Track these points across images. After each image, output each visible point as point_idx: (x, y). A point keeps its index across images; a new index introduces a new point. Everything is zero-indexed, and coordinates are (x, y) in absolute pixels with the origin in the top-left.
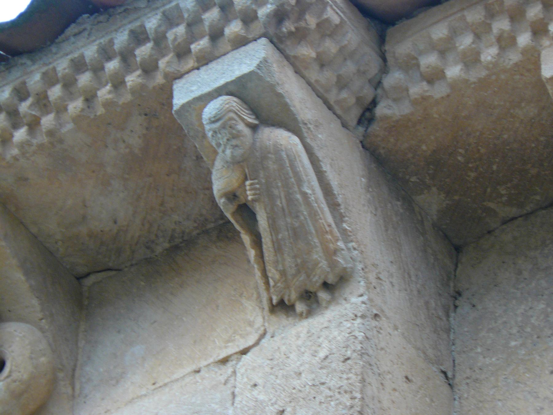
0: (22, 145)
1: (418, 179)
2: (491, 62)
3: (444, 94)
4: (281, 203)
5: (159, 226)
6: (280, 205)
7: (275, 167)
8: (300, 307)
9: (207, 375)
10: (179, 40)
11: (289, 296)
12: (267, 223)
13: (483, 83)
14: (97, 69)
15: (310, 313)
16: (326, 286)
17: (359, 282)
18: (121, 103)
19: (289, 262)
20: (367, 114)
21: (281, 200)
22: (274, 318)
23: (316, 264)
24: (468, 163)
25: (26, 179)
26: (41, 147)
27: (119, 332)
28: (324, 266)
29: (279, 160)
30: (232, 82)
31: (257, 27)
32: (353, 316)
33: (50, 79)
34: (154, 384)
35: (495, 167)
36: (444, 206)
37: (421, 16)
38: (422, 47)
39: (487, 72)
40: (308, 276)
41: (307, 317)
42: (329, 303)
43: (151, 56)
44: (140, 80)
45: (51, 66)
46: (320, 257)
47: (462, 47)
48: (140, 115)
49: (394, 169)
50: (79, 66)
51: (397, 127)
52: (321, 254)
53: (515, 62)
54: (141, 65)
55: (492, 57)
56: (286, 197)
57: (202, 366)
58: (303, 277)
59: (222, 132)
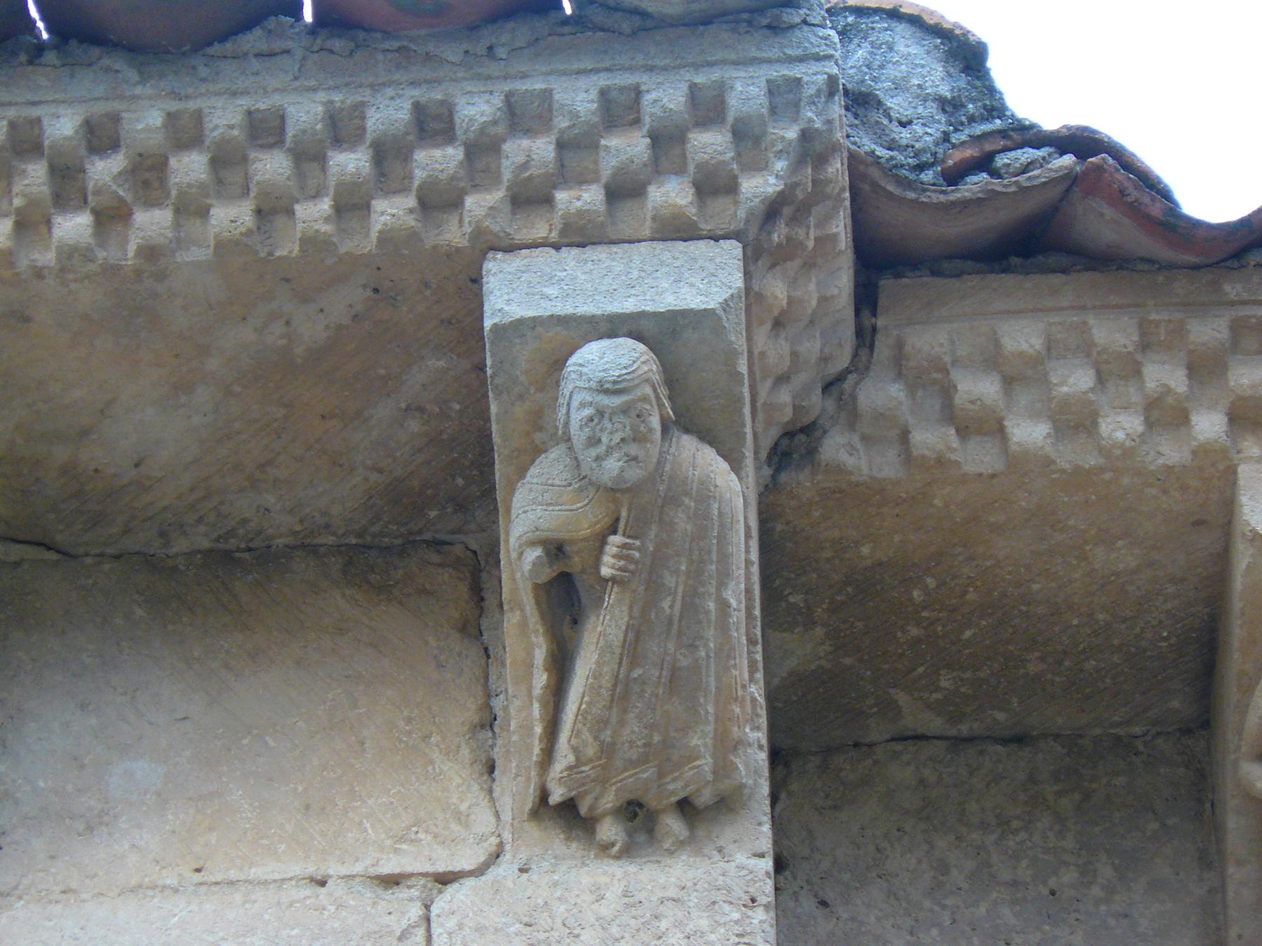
0: (70, 253)
1: (806, 601)
2: (1122, 446)
3: (986, 469)
4: (671, 607)
5: (222, 503)
6: (668, 611)
7: (689, 527)
8: (609, 830)
9: (352, 902)
10: (533, 171)
11: (596, 799)
12: (621, 637)
13: (1079, 478)
14: (309, 156)
15: (627, 852)
16: (685, 807)
17: (760, 824)
18: (342, 250)
19: (633, 732)
21: (674, 601)
22: (533, 830)
23: (693, 756)
24: (925, 608)
25: (27, 319)
26: (110, 270)
27: (83, 706)
28: (706, 769)
29: (701, 516)
30: (655, 315)
31: (726, 213)
32: (746, 898)
33: (185, 133)
34: (198, 870)
35: (968, 634)
36: (813, 667)
37: (973, 281)
38: (962, 351)
39: (1101, 461)
40: (661, 775)
41: (617, 857)
42: (681, 844)
43: (453, 178)
44: (411, 221)
45: (192, 105)
46: (705, 745)
47: (1065, 389)
48: (365, 287)
50: (266, 130)
51: (849, 494)
52: (709, 741)
53: (1169, 463)
54: (420, 188)
55: (1127, 435)
56: (683, 597)
57: (331, 872)
58: (648, 773)
59: (615, 419)
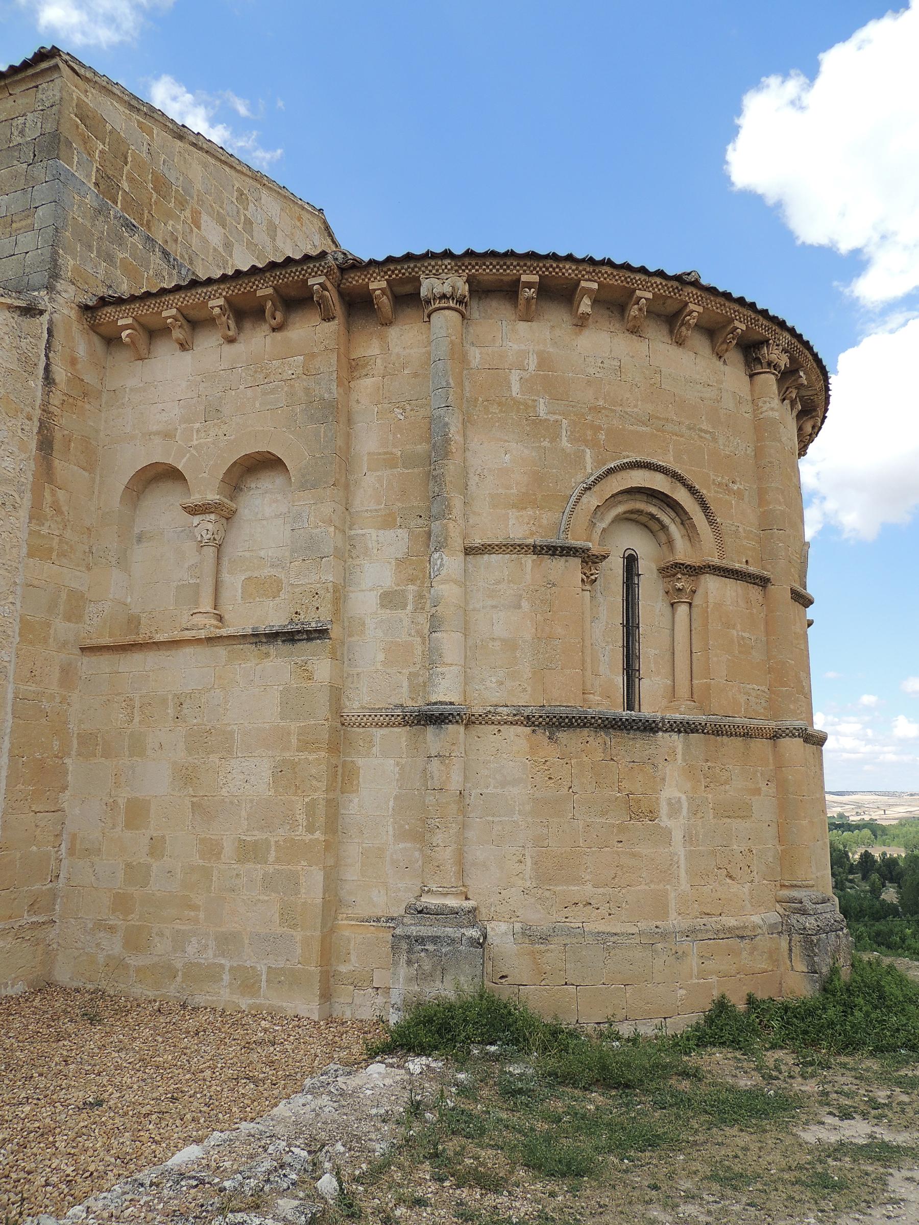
20: (339, 286)
49: (341, 294)
